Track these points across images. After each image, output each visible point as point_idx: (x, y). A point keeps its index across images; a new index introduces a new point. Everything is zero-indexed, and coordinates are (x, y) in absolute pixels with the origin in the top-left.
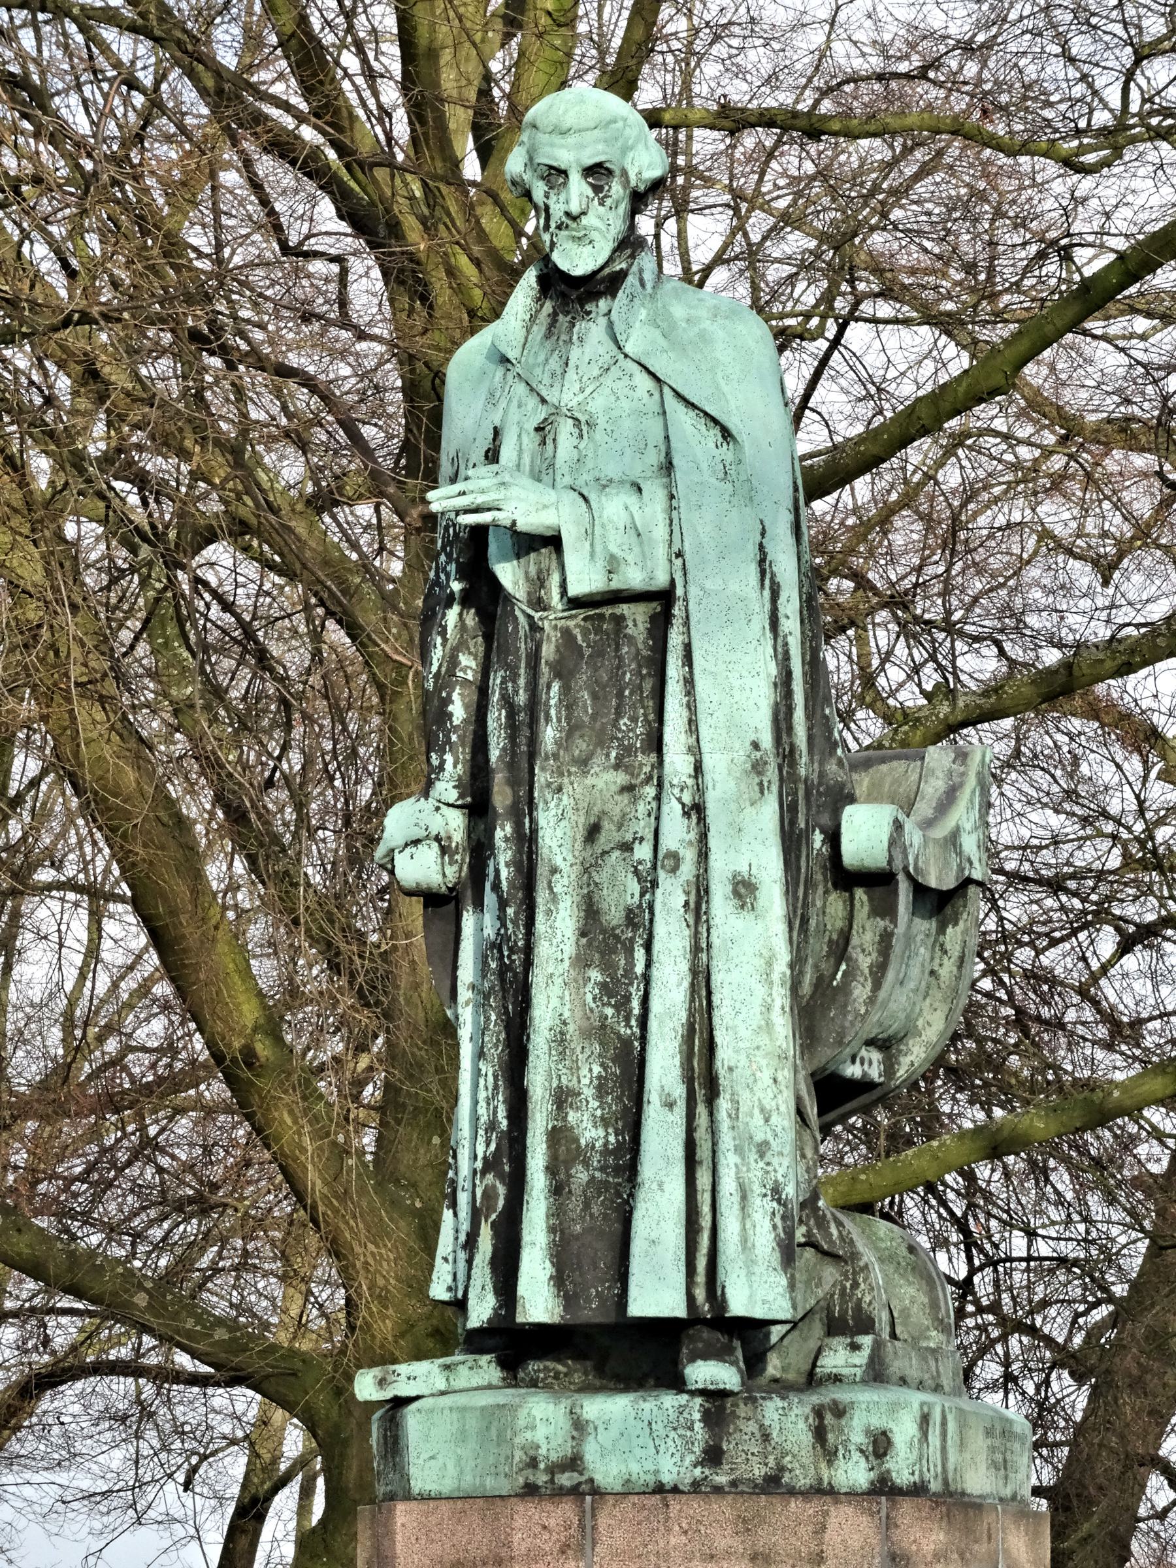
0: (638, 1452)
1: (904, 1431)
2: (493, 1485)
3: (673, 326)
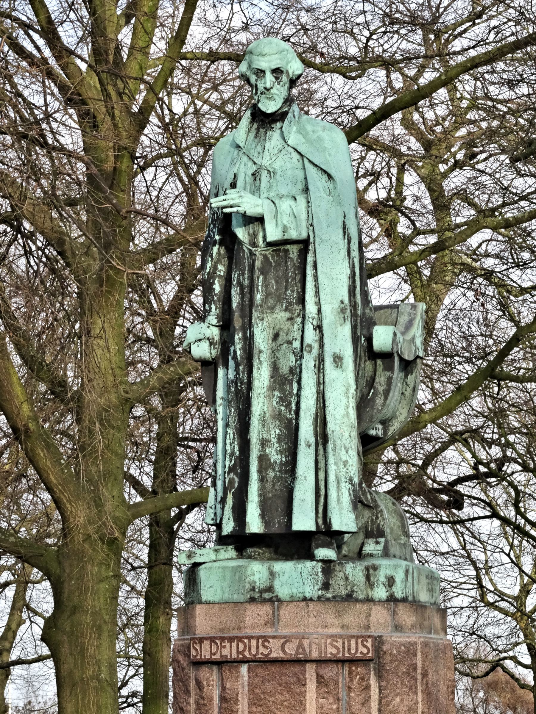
1: (399, 576)
2: (236, 597)
3: (307, 133)
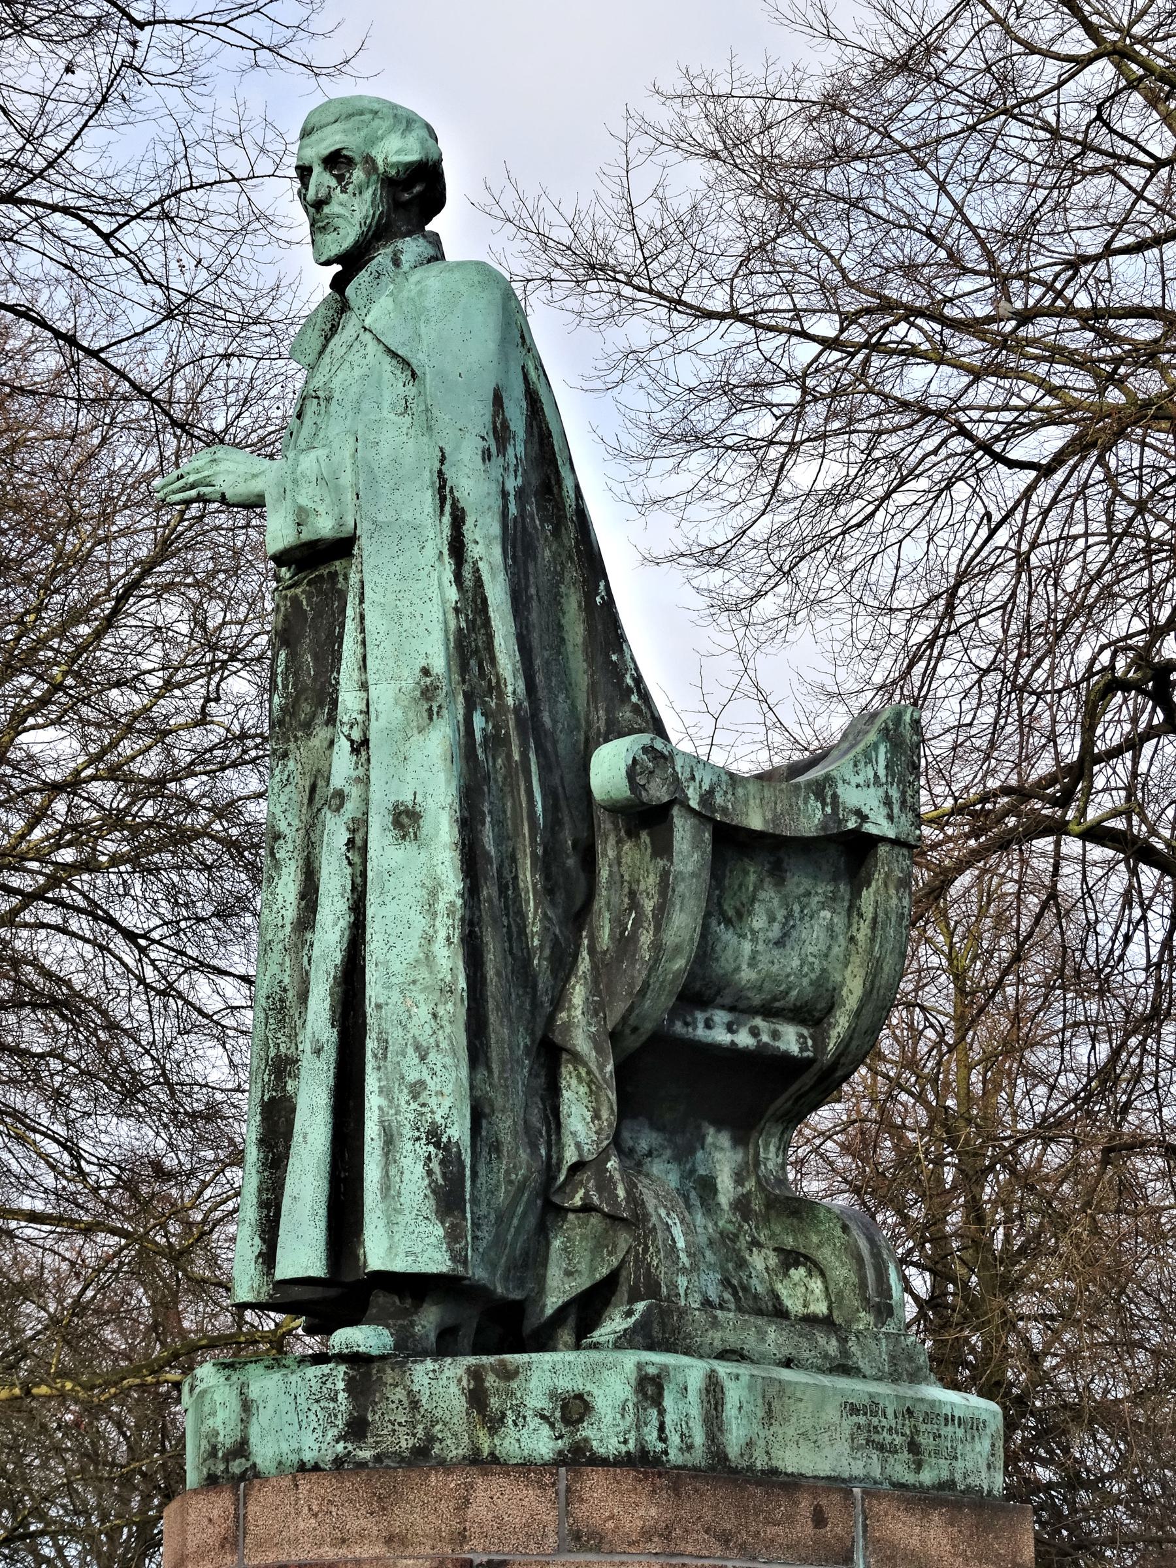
0: (288, 1430)
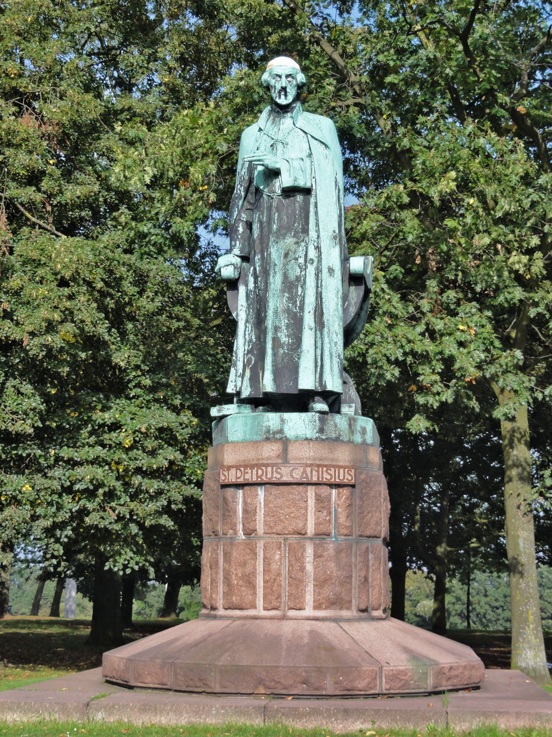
2: (255, 438)
